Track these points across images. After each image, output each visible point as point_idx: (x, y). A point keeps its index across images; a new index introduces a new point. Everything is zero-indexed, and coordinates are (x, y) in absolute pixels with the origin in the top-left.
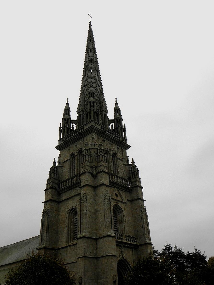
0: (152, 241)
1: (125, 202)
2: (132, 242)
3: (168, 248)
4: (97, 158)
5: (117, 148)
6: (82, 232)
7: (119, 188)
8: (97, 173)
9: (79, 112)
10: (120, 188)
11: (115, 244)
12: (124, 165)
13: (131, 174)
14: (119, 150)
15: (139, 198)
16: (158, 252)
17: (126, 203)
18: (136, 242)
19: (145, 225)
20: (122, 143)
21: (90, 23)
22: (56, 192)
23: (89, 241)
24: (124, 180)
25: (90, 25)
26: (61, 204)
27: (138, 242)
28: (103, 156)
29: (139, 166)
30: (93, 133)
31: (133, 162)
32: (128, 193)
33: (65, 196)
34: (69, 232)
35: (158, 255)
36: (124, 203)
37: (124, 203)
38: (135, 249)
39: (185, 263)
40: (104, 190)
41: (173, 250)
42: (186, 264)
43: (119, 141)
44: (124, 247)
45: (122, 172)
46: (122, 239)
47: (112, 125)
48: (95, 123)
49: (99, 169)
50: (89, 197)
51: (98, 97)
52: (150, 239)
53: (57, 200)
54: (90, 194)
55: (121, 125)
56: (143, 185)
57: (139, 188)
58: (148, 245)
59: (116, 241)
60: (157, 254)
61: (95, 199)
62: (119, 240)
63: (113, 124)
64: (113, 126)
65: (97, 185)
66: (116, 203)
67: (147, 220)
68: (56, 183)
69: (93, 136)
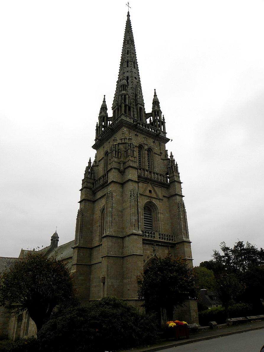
0: (191, 239)
1: (161, 198)
2: (167, 240)
3: (240, 244)
4: (125, 153)
5: (154, 142)
6: (106, 231)
7: (153, 183)
8: (125, 169)
9: (114, 108)
10: (155, 184)
11: (141, 242)
12: (162, 159)
13: (169, 169)
14: (156, 144)
15: (177, 193)
16: (230, 249)
17: (162, 200)
18: (172, 241)
19: (182, 222)
20: (159, 136)
21: (128, 13)
22: (91, 192)
23: (114, 239)
24: (159, 176)
25: (128, 16)
26: (96, 203)
27: (175, 241)
28: (131, 150)
29: (178, 160)
30: (123, 127)
31: (172, 156)
32: (165, 189)
33: (99, 194)
34: (101, 231)
35: (230, 252)
36: (159, 199)
37: (159, 199)
38: (171, 247)
39: (258, 259)
40: (130, 186)
41: (245, 247)
42: (259, 260)
43: (155, 134)
44: (157, 245)
45: (159, 166)
46: (154, 237)
47: (150, 119)
48: (126, 117)
49: (127, 165)
50: (115, 194)
51: (133, 90)
52: (187, 237)
53: (92, 200)
54: (117, 191)
55: (160, 117)
56: (182, 179)
57: (176, 183)
58: (185, 243)
59: (143, 239)
60: (229, 251)
61: (122, 196)
62: (161, 240)
63: (151, 118)
64: (152, 120)
65: (124, 181)
66: (149, 200)
67: (186, 217)
68: (91, 183)
69: (123, 130)
